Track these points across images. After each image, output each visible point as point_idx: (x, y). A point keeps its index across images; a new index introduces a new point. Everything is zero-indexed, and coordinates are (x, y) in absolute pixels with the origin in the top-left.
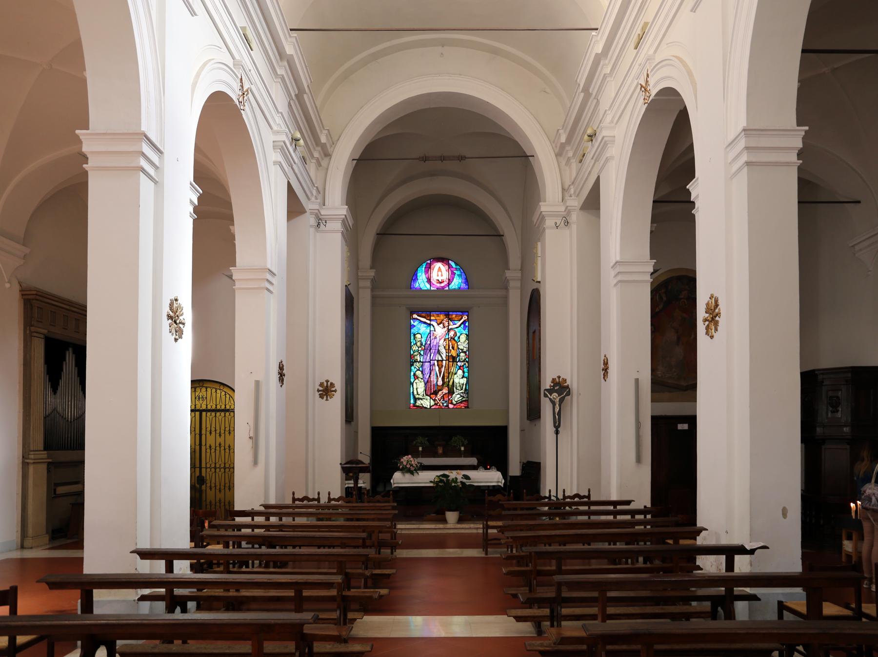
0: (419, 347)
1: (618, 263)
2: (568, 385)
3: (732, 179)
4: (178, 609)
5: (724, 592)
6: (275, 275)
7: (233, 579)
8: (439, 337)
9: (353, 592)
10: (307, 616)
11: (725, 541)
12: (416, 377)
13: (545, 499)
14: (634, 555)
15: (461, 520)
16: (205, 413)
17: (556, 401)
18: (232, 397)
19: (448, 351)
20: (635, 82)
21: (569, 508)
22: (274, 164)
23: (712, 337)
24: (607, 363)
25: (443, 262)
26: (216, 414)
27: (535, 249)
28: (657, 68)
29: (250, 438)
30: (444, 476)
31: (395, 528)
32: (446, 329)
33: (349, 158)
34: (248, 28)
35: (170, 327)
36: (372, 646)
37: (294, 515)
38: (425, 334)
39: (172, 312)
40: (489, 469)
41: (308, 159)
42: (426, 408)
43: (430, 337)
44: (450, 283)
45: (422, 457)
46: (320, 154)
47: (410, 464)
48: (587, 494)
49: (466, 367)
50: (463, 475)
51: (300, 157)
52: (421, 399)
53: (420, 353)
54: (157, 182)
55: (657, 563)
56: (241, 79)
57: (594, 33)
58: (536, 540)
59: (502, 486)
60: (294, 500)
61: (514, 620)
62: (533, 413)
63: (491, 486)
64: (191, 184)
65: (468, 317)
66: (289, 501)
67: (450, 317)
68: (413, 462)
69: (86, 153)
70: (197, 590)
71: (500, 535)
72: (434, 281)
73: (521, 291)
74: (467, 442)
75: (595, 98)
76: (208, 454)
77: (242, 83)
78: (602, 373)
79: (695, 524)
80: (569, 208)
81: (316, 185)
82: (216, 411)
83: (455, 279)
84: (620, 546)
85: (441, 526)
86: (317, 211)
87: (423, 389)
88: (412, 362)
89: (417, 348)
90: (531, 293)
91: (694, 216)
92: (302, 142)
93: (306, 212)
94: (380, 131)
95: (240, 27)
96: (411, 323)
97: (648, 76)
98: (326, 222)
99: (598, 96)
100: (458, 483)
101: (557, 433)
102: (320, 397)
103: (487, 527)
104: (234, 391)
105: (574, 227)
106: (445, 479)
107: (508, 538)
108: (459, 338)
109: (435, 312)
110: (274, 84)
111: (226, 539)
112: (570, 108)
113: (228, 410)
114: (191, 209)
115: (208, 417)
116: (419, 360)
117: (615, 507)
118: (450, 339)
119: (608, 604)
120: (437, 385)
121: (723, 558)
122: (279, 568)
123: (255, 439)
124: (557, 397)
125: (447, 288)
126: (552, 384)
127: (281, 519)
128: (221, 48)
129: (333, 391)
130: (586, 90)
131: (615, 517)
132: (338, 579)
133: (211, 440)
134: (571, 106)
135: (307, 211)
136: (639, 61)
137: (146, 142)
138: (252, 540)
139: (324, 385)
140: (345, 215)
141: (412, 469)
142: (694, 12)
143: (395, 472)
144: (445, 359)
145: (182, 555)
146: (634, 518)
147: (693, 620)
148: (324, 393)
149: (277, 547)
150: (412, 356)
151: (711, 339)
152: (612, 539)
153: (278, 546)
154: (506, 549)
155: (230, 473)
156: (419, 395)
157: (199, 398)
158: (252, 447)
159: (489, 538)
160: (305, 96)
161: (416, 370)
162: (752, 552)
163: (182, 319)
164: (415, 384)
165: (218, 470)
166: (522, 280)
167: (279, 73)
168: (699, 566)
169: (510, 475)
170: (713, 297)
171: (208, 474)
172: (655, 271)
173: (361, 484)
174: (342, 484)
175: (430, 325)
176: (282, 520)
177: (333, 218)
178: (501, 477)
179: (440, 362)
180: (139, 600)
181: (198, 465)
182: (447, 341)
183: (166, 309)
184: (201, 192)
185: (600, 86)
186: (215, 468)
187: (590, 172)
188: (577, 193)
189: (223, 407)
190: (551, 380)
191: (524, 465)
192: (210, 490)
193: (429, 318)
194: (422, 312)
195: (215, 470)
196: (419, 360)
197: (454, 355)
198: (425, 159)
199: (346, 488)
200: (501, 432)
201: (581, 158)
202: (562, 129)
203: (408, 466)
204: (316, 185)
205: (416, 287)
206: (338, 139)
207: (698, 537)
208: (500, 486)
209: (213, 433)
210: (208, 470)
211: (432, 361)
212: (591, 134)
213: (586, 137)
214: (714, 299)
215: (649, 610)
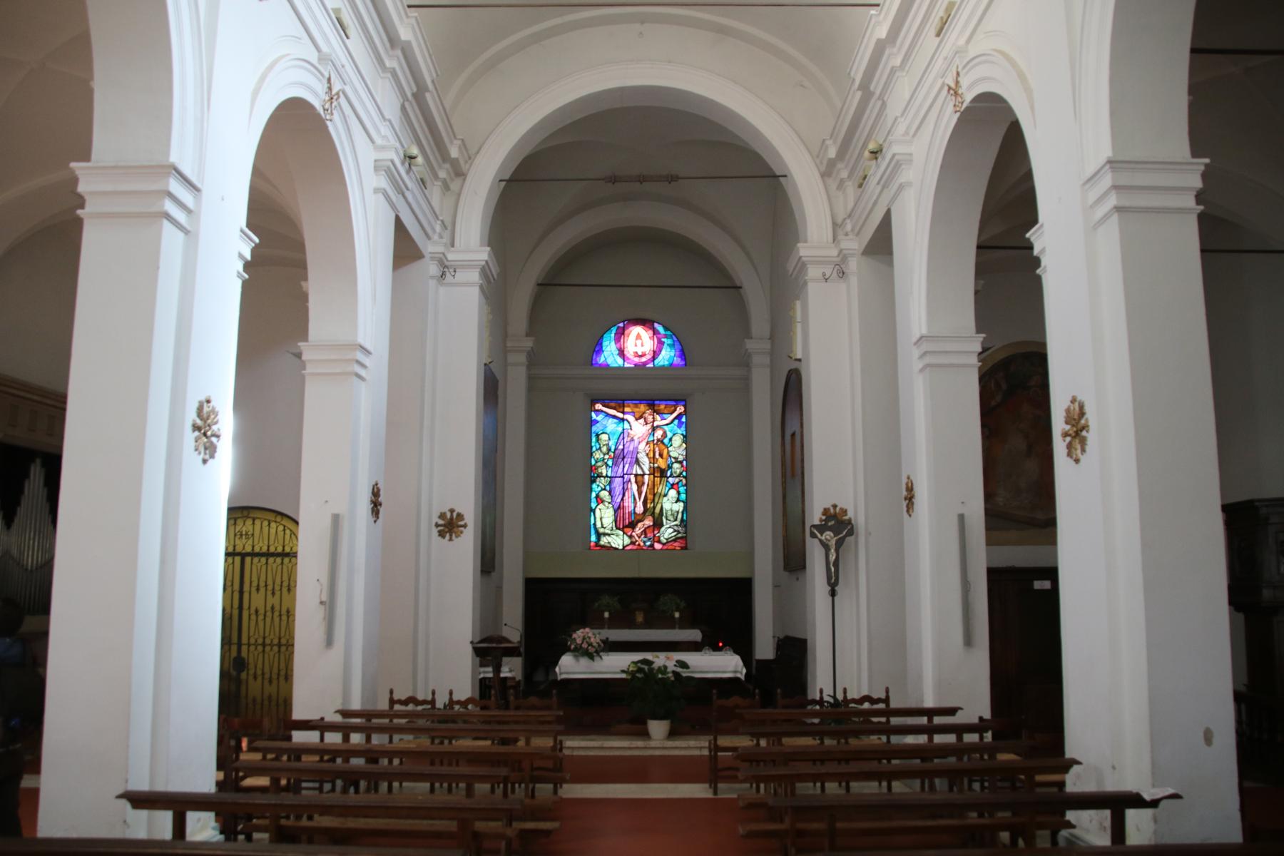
0: (604, 455)
1: (924, 339)
8: (639, 438)
11: (1112, 785)
12: (600, 500)
15: (673, 734)
17: (830, 544)
18: (294, 534)
19: (653, 460)
23: (1077, 461)
28: (971, 64)
29: (321, 603)
32: (649, 426)
33: (495, 177)
35: (196, 441)
37: (391, 730)
38: (614, 434)
39: (201, 420)
42: (616, 549)
43: (623, 439)
45: (609, 628)
46: (448, 173)
47: (587, 642)
48: (883, 696)
49: (683, 486)
50: (677, 661)
51: (417, 180)
53: (606, 463)
56: (329, 80)
57: (873, 11)
60: (392, 702)
62: (793, 562)
64: (242, 231)
65: (685, 408)
66: (383, 705)
67: (656, 408)
68: (592, 640)
69: (83, 194)
73: (772, 372)
75: (879, 99)
76: (253, 623)
77: (330, 84)
78: (905, 504)
80: (844, 252)
81: (441, 218)
82: (268, 555)
83: (663, 352)
85: (640, 743)
86: (441, 255)
88: (594, 477)
89: (602, 456)
90: (788, 376)
92: (420, 160)
95: (332, 9)
96: (591, 417)
97: (958, 74)
98: (455, 271)
100: (668, 673)
101: (833, 594)
104: (297, 523)
105: (854, 280)
106: (646, 668)
108: (671, 440)
109: (632, 400)
113: (288, 555)
114: (240, 266)
115: (253, 565)
116: (604, 474)
118: (655, 442)
120: (635, 513)
121: (1107, 813)
123: (329, 605)
125: (651, 365)
126: (824, 518)
129: (462, 526)
130: (865, 87)
133: (258, 600)
135: (425, 254)
136: (944, 54)
140: (487, 262)
141: (591, 650)
145: (198, 802)
148: (447, 530)
150: (593, 468)
155: (290, 565)
156: (605, 528)
157: (241, 535)
160: (428, 95)
161: (600, 489)
162: (1154, 804)
164: (597, 511)
165: (268, 648)
166: (772, 353)
171: (251, 655)
172: (984, 350)
173: (507, 672)
174: (474, 673)
175: (623, 420)
177: (467, 266)
178: (741, 663)
179: (639, 478)
181: (235, 639)
182: (652, 445)
183: (191, 416)
184: (257, 240)
185: (886, 83)
187: (875, 203)
189: (280, 550)
190: (822, 510)
191: (780, 643)
192: (256, 592)
196: (604, 474)
198: (613, 180)
200: (741, 589)
201: (861, 181)
202: (831, 138)
203: (585, 646)
204: (441, 218)
206: (478, 152)
208: (738, 679)
209: (262, 590)
210: (252, 648)
212: (875, 150)
213: (867, 154)
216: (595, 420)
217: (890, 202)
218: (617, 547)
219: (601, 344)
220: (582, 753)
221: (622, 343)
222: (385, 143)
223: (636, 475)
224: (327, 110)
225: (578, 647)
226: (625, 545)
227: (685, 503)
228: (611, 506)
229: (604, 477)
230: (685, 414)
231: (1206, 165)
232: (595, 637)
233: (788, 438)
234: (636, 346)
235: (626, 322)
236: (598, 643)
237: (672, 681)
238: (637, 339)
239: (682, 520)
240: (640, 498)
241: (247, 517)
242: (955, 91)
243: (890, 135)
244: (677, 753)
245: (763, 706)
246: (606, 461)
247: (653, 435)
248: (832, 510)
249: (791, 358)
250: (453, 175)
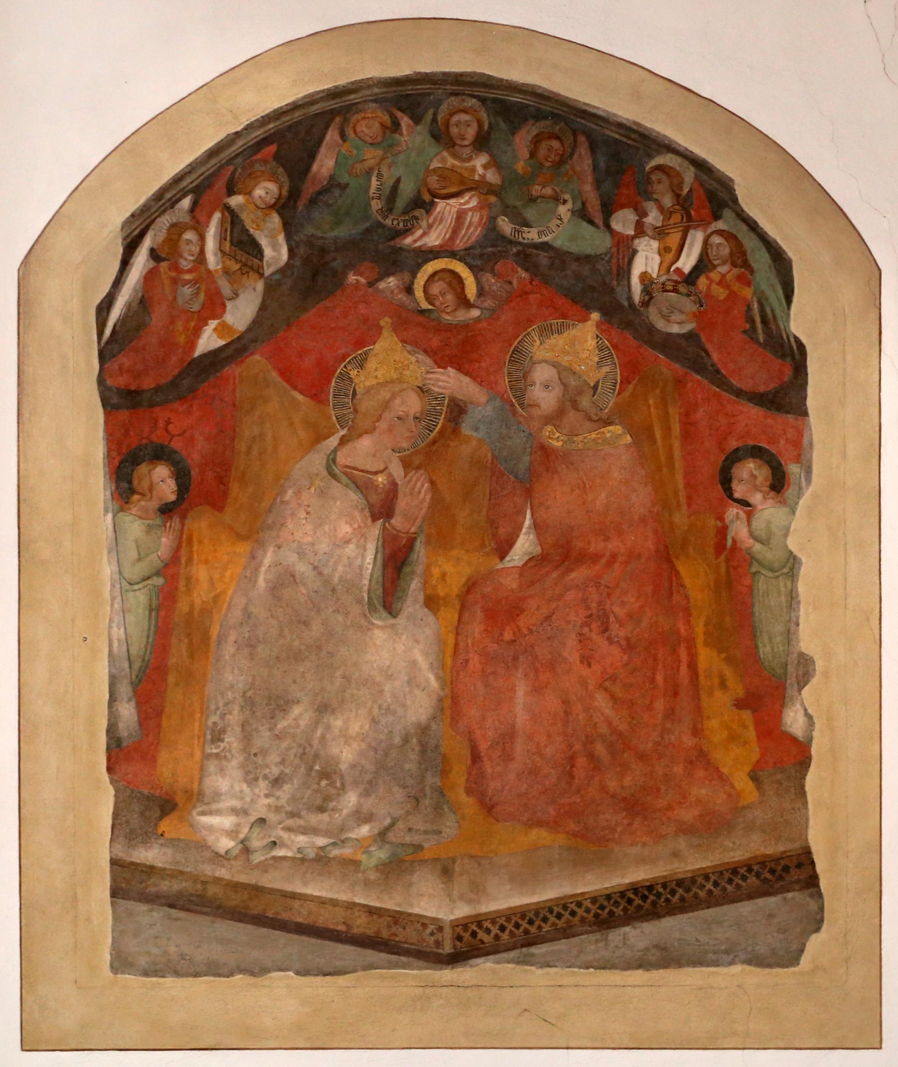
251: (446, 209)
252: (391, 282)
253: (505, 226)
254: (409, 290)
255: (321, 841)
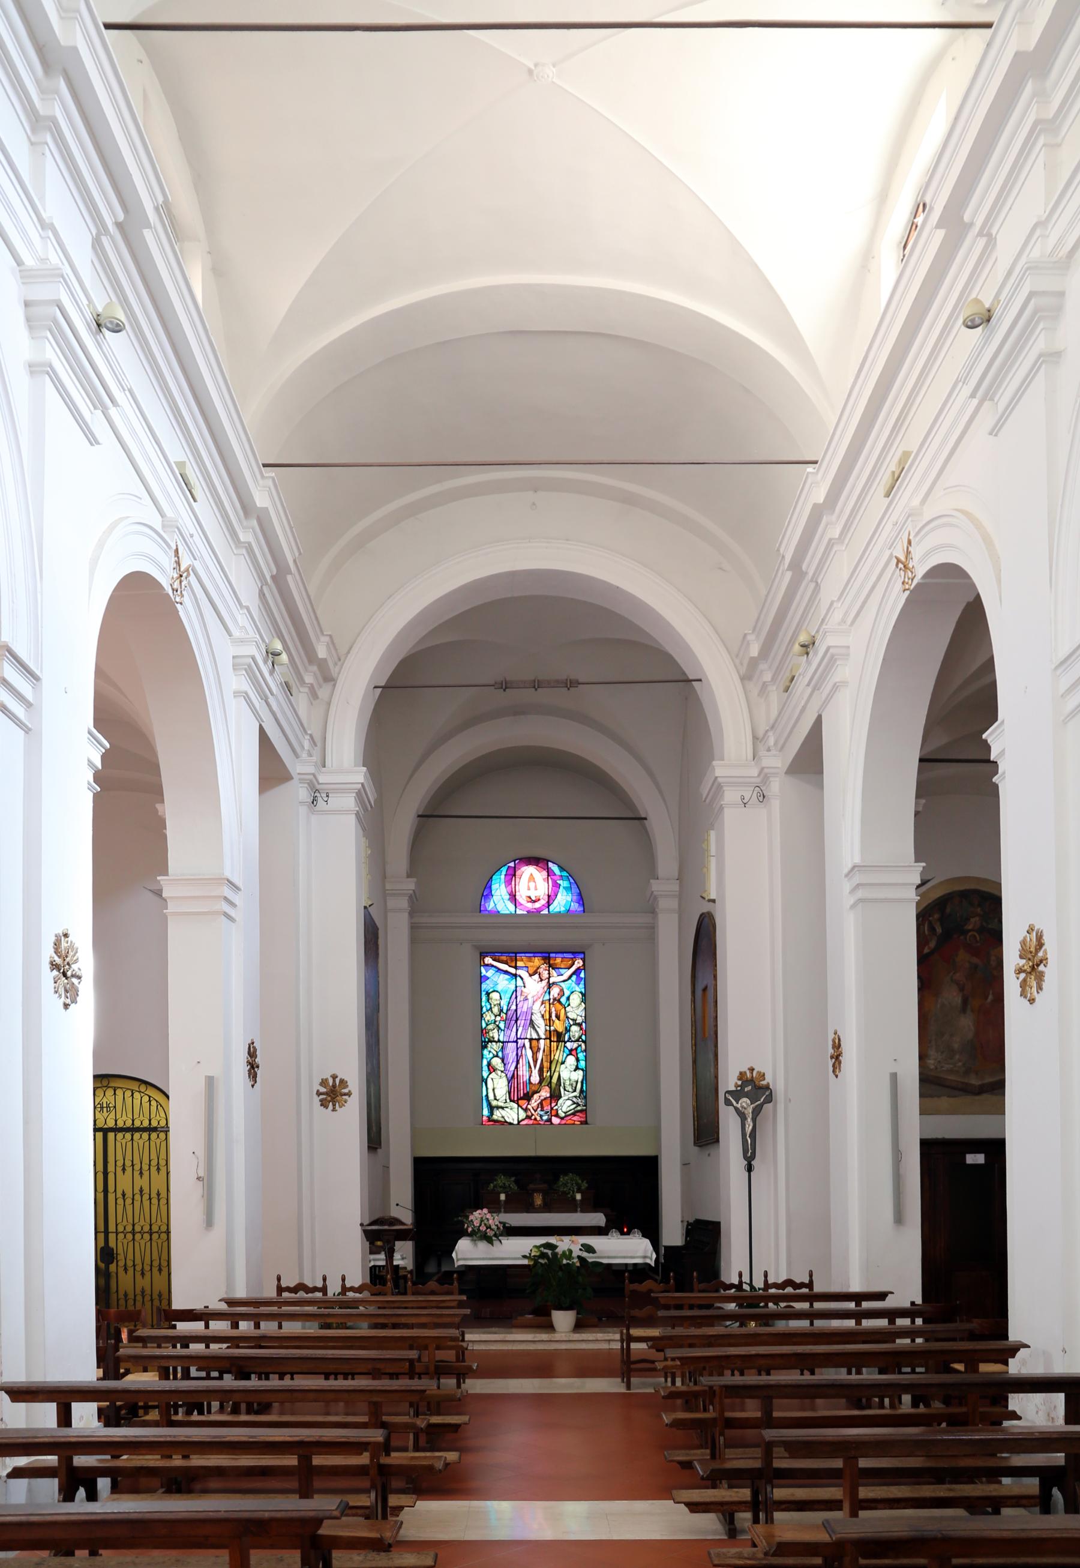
0: (496, 1016)
1: (856, 869)
2: (768, 1083)
3: (1066, 723)
4: (81, 1493)
5: (1063, 1460)
6: (238, 889)
7: (186, 1437)
9: (396, 1458)
10: (322, 1504)
12: (492, 1069)
13: (731, 1289)
14: (895, 1391)
16: (113, 1134)
17: (746, 1112)
19: (549, 1022)
20: (887, 553)
21: (775, 1304)
22: (235, 696)
23: (1032, 1001)
24: (839, 1045)
25: (537, 866)
26: (132, 1135)
27: (706, 843)
29: (198, 1178)
30: (548, 1246)
31: (463, 1340)
32: (544, 983)
34: (188, 463)
35: (55, 983)
36: (436, 1555)
37: (279, 1318)
39: (59, 957)
40: (628, 1233)
41: (294, 685)
42: (511, 1124)
43: (516, 997)
44: (551, 901)
45: (506, 1212)
47: (485, 1224)
49: (582, 1051)
50: (582, 1245)
51: (281, 683)
52: (502, 1108)
53: (498, 1026)
54: (30, 729)
55: (937, 1406)
56: (177, 551)
57: (810, 469)
58: (721, 1364)
59: (653, 1265)
60: (280, 1290)
61: (686, 1509)
63: (630, 1264)
64: (90, 733)
65: (584, 962)
66: (271, 1293)
70: (112, 1457)
71: (653, 1354)
72: (521, 898)
74: (587, 1185)
75: (811, 581)
76: (120, 1208)
77: (178, 558)
78: (831, 1063)
79: (1006, 1338)
80: (766, 770)
81: (309, 732)
82: (133, 1130)
84: (870, 1375)
85: (544, 1336)
87: (505, 1089)
88: (485, 1042)
91: (996, 787)
92: (284, 657)
93: (292, 778)
94: (425, 636)
95: (174, 462)
96: (481, 973)
97: (909, 542)
99: (818, 576)
100: (573, 1258)
101: (750, 1169)
102: (321, 1105)
103: (631, 1339)
104: (168, 1097)
105: (776, 804)
106: (549, 1252)
107: (673, 1359)
108: (568, 999)
109: (525, 953)
110: (234, 557)
111: (164, 1363)
112: (767, 596)
114: (90, 777)
116: (496, 1039)
117: (858, 1304)
118: (551, 1001)
119: (861, 1481)
120: (530, 1083)
122: (257, 1413)
123: (207, 1181)
124: (748, 1105)
125: (545, 912)
126: (740, 1083)
127: (257, 1326)
128: (141, 499)
130: (796, 565)
131: (858, 1323)
132: (377, 1435)
133: (124, 1182)
134: (768, 593)
136: (894, 518)
137: (10, 660)
138: (210, 1364)
139: (328, 1083)
140: (362, 784)
141: (490, 1233)
142: (996, 435)
143: (459, 1238)
144: (543, 1036)
145: (84, 1394)
146: (894, 1323)
147: (1006, 1511)
148: (329, 1098)
149: (253, 1376)
150: (483, 1032)
151: (1031, 1004)
152: (854, 1362)
153: (253, 1373)
154: (663, 1379)
158: (203, 1196)
159: (633, 1359)
160: (289, 578)
161: (491, 1055)
163: (76, 970)
164: (489, 1081)
165: (138, 1236)
166: (681, 896)
167: (242, 540)
168: (1014, 1412)
169: (664, 1244)
170: (1032, 930)
171: (120, 1245)
172: (923, 883)
173: (399, 1260)
174: (364, 1259)
175: (515, 976)
176: (259, 1328)
179: (534, 1043)
180: (10, 1476)
183: (48, 953)
184: (108, 745)
186: (133, 1233)
188: (779, 746)
189: (146, 1124)
190: (738, 1074)
193: (514, 964)
194: (502, 953)
195: (134, 1236)
196: (496, 1039)
197: (560, 1029)
198: (504, 686)
199: (371, 1268)
201: (788, 684)
204: (309, 732)
205: (489, 909)
206: (348, 652)
207: (1010, 1360)
209: (129, 1170)
210: (121, 1236)
211: (519, 1041)
212: (806, 643)
213: (797, 648)
214: (1034, 933)
215: (928, 1491)
216: (485, 975)
217: (820, 709)
218: (512, 1121)
219: (490, 887)
220: (483, 1347)
221: (513, 886)
222: (243, 635)
223: (531, 1040)
224: (177, 591)
225: (476, 1229)
226: (520, 1119)
227: (585, 1071)
228: (503, 1075)
229: (496, 1042)
230: (584, 969)
231: (924, 867)
232: (494, 1219)
233: (699, 993)
234: (529, 889)
235: (517, 862)
236: (497, 1225)
237: (578, 1267)
238: (529, 881)
239: (582, 1091)
240: (535, 1067)
241: (108, 1087)
242: (904, 565)
243: (824, 624)
244: (584, 1346)
245: (678, 1290)
246: (497, 1023)
247: (549, 993)
248: (749, 1075)
249: (703, 898)
250: (321, 680)
251: (973, 920)
252: (962, 937)
253: (984, 924)
254: (966, 939)
255: (951, 1066)
